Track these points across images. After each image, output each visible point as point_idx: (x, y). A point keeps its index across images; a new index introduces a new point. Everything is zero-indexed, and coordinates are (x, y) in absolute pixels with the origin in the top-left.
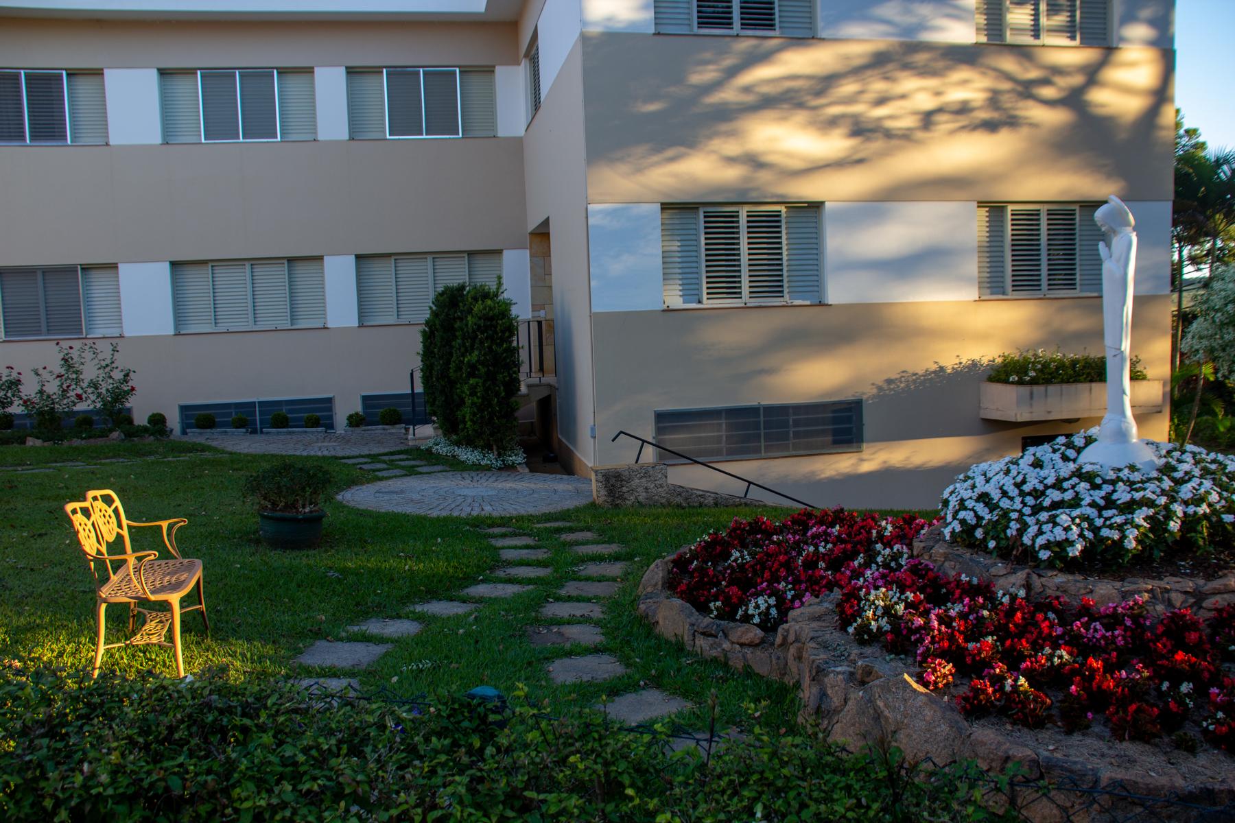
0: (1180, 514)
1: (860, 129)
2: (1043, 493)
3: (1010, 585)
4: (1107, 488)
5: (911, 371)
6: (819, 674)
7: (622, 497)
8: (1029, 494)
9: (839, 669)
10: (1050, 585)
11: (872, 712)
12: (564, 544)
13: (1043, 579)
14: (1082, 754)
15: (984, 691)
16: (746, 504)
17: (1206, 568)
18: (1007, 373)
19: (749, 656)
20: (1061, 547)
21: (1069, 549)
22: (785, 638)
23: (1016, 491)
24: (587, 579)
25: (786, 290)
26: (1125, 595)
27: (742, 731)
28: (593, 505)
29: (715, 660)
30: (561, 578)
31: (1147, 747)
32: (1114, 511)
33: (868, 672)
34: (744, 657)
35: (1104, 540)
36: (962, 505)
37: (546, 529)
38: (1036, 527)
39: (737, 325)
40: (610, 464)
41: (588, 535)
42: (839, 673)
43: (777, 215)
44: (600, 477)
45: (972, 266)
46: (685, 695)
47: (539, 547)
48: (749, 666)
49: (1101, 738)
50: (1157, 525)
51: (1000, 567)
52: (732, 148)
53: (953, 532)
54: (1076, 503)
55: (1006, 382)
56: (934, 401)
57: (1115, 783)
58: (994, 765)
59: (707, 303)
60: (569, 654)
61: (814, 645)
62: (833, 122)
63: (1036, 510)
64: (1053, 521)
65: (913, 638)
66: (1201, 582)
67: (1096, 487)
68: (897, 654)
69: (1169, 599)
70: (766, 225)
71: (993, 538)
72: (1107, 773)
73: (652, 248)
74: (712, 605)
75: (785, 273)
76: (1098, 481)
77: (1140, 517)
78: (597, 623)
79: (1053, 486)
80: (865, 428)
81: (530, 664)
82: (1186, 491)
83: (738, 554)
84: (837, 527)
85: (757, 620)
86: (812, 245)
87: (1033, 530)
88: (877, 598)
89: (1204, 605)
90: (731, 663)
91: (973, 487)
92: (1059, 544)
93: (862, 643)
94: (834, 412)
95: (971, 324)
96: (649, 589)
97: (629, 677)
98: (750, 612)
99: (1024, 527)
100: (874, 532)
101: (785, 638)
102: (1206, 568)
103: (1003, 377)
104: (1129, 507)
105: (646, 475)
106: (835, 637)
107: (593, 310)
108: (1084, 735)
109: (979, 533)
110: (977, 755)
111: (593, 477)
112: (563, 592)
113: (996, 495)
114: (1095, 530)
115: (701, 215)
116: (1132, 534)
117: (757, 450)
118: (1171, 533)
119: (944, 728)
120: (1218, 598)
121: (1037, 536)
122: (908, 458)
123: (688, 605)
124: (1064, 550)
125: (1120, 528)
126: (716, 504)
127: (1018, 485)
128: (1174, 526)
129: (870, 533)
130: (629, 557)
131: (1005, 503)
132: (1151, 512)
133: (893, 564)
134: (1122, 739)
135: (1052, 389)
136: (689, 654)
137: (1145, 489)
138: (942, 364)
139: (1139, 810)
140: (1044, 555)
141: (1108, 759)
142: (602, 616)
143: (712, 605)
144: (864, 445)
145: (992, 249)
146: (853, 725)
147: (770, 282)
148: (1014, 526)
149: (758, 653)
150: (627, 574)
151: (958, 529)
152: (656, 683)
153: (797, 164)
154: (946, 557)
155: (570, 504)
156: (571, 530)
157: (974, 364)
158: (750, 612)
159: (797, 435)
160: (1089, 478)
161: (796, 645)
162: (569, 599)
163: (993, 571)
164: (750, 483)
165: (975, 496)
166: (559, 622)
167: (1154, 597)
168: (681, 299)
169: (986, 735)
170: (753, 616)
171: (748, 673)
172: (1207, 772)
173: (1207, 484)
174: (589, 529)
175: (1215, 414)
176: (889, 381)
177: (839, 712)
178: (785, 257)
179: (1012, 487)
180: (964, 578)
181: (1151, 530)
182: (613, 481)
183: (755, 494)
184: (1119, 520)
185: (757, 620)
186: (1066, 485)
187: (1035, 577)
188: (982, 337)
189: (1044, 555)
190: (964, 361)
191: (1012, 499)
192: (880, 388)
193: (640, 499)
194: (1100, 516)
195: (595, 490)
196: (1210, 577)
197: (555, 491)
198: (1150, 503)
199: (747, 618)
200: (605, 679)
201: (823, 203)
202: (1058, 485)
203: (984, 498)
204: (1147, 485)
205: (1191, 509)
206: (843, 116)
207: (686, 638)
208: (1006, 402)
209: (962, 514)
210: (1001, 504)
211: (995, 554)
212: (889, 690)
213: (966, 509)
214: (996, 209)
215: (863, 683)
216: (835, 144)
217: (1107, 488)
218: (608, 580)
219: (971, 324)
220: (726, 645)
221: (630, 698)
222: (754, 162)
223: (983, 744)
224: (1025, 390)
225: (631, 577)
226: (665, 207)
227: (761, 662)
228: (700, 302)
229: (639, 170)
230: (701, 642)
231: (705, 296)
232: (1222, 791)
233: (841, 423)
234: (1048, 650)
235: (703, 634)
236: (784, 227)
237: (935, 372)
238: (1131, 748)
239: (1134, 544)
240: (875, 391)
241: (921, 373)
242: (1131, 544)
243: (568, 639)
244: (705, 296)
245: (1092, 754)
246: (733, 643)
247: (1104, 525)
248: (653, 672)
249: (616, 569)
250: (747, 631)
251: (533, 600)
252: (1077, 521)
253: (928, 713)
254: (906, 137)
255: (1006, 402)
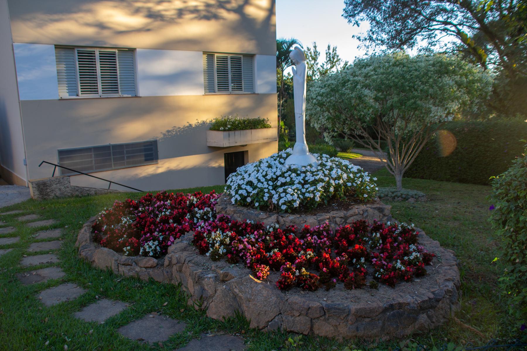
0: (334, 184)
1: (151, 15)
2: (276, 179)
3: (270, 222)
4: (303, 175)
5: (177, 126)
6: (198, 280)
7: (47, 194)
8: (270, 180)
9: (209, 276)
10: (287, 220)
11: (231, 295)
12: (22, 223)
13: (284, 218)
14: (339, 300)
15: (289, 278)
16: (110, 193)
17: (343, 206)
18: (218, 126)
19: (151, 273)
20: (290, 203)
21: (294, 204)
22: (170, 262)
23: (264, 179)
24: (42, 241)
25: (120, 90)
26: (319, 222)
27: (161, 314)
28: (32, 200)
29: (132, 278)
30: (27, 242)
31: (361, 290)
32: (309, 185)
33: (226, 275)
34: (148, 274)
35: (306, 198)
36: (239, 187)
37: (9, 215)
38: (277, 195)
39: (96, 107)
40: (38, 178)
41: (34, 216)
42: (210, 278)
43: (114, 54)
44: (34, 185)
45: (202, 79)
46: (123, 299)
47: (8, 226)
48: (152, 278)
49: (341, 290)
50: (326, 189)
51: (262, 215)
52: (89, 18)
53: (236, 200)
54: (292, 183)
55: (218, 130)
56: (186, 140)
57: (357, 311)
58: (303, 312)
59: (81, 96)
60: (48, 286)
61: (191, 265)
62: (137, 11)
63: (275, 188)
64: (285, 191)
65: (241, 255)
66: (345, 212)
67: (298, 175)
68: (235, 263)
69: (336, 221)
70: (109, 58)
71: (257, 202)
72: (354, 307)
73: (51, 68)
74: (125, 249)
75: (119, 82)
76: (299, 172)
77: (320, 186)
78: (58, 266)
79: (280, 176)
80: (159, 153)
81: (27, 297)
82: (334, 173)
83: (125, 220)
84: (169, 201)
85: (151, 254)
86: (131, 68)
87: (276, 197)
88: (216, 236)
89: (348, 222)
90: (141, 278)
91: (243, 179)
92: (290, 202)
93: (215, 260)
94: (145, 146)
95: (202, 105)
96: (84, 243)
97: (89, 295)
98: (147, 250)
99: (271, 197)
100: (188, 202)
101: (170, 262)
102: (343, 206)
103: (217, 128)
104: (314, 183)
105: (59, 182)
106: (199, 258)
107: (21, 99)
108: (334, 290)
109: (249, 200)
110: (293, 309)
111: (30, 186)
112: (31, 250)
113: (255, 182)
114: (303, 194)
115: (76, 52)
116: (318, 195)
117: (110, 166)
118: (331, 193)
119: (274, 298)
120: (352, 218)
121: (279, 199)
122: (178, 165)
123: (111, 250)
124: (292, 204)
125: (313, 192)
126: (96, 194)
127: (264, 177)
128: (332, 189)
129: (186, 203)
130: (62, 226)
131: (260, 185)
132: (323, 184)
133: (205, 217)
134: (351, 289)
135: (237, 133)
136: (117, 277)
137: (318, 175)
138: (191, 123)
139: (367, 320)
140: (284, 207)
141: (349, 300)
142: (58, 261)
143: (125, 249)
144: (159, 161)
145: (209, 71)
146: (221, 302)
147: (112, 87)
148: (267, 195)
149: (156, 271)
150: (64, 235)
151: (239, 198)
152: (105, 295)
153: (123, 29)
154: (235, 212)
155: (18, 200)
156: (23, 215)
157: (204, 123)
158: (147, 250)
159: (128, 157)
160: (295, 171)
161: (178, 265)
162: (36, 254)
163: (260, 216)
164: (111, 182)
165: (245, 182)
166: (35, 268)
167: (330, 221)
168: (68, 94)
169: (296, 298)
170: (149, 252)
171: (152, 282)
172: (386, 296)
173: (340, 172)
174: (33, 213)
175: (285, 141)
176: (168, 131)
177: (212, 297)
178: (118, 74)
179: (262, 178)
180: (248, 222)
181: (324, 192)
182: (42, 187)
183: (114, 187)
184: (312, 189)
185: (151, 254)
186: (286, 175)
187: (280, 218)
188: (206, 110)
189: (284, 207)
190: (200, 122)
191: (262, 183)
192: (164, 135)
193: (57, 194)
194: (303, 188)
195: (32, 192)
196: (347, 209)
197: (7, 195)
198: (322, 181)
199: (146, 254)
200: (75, 298)
201: (135, 49)
202: (283, 175)
203: (250, 183)
204: (318, 172)
205: (337, 182)
206: (142, 8)
207: (113, 268)
208: (219, 139)
209: (240, 192)
210: (258, 186)
211: (258, 209)
212: (242, 284)
213: (242, 189)
214: (210, 55)
215: (223, 281)
216: (138, 21)
217: (303, 175)
218: (54, 240)
219: (202, 105)
220: (138, 269)
221: (93, 307)
222: (102, 26)
223: (296, 303)
224: (226, 133)
225: (66, 237)
226: (58, 47)
227: (158, 275)
228: (77, 95)
229: (40, 26)
230: (122, 269)
231: (80, 93)
232: (396, 304)
233: (149, 151)
234: (302, 252)
235: (123, 265)
236: (117, 59)
237: (188, 127)
238: (357, 292)
239: (319, 199)
240: (162, 136)
241: (182, 127)
242: (318, 199)
243: (44, 277)
244: (80, 93)
245: (339, 297)
246: (141, 267)
247: (306, 192)
248: (101, 289)
249: (57, 233)
250: (149, 260)
251: (15, 257)
252: (296, 191)
253: (265, 293)
254: (171, 21)
255: (219, 139)
